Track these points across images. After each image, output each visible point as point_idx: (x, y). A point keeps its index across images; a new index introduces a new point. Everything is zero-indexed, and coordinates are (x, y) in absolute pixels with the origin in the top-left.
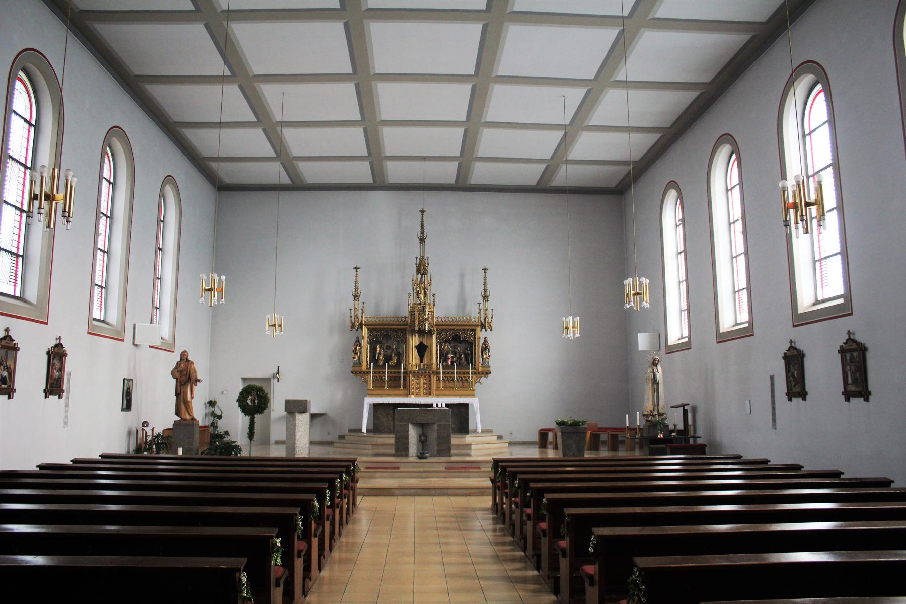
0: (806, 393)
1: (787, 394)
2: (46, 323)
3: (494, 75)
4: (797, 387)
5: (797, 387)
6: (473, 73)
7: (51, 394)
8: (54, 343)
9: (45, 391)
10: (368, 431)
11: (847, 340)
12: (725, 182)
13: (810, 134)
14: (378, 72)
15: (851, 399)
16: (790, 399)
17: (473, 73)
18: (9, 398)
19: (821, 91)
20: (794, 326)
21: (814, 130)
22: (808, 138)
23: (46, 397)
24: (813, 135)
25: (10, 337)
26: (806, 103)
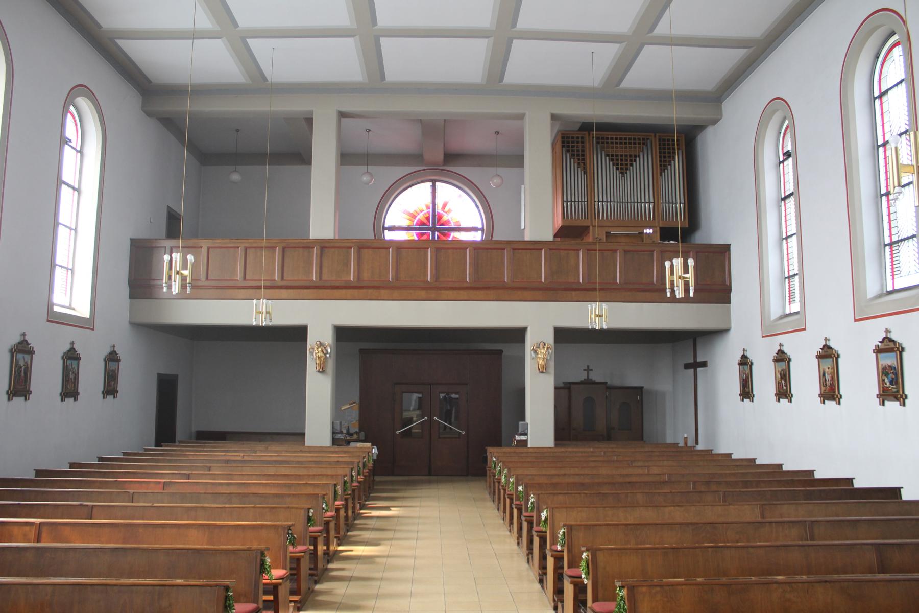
0: (78, 394)
1: (776, 395)
2: (93, 329)
3: (492, 39)
4: (20, 386)
5: (20, 386)
6: (515, 41)
7: (14, 395)
8: (68, 347)
9: (7, 392)
10: (565, 431)
11: (884, 339)
12: (72, 108)
13: (881, 96)
14: (351, 40)
15: (886, 402)
16: (743, 400)
17: (515, 41)
18: (26, 400)
19: (896, 44)
20: (856, 320)
21: (886, 92)
22: (877, 102)
23: (62, 400)
24: (884, 98)
25: (26, 341)
26: (877, 57)
